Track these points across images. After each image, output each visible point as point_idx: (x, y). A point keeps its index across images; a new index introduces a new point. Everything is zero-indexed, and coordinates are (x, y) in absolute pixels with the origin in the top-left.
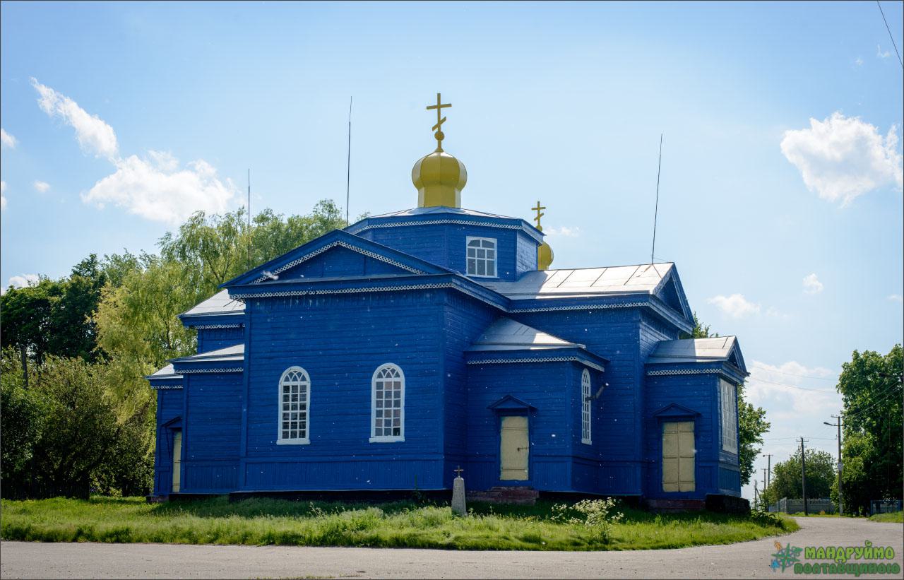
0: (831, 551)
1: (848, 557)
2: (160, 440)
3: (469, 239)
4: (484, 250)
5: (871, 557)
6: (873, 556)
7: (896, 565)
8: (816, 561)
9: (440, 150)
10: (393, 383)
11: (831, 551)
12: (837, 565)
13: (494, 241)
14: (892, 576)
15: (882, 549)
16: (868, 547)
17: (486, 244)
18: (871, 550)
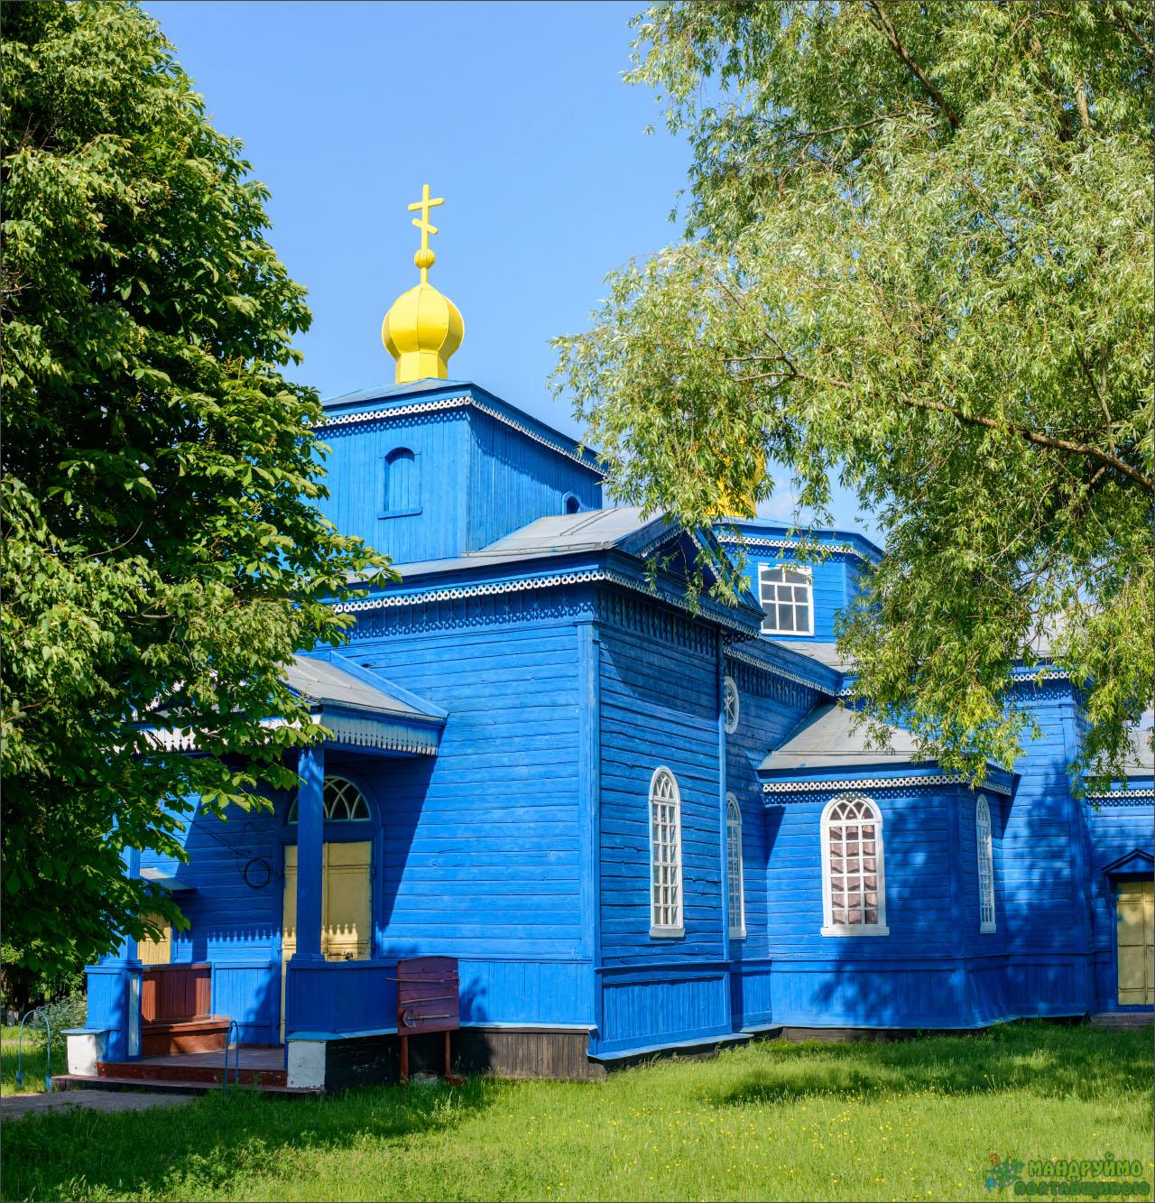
16: (1109, 1162)
18: (1112, 1164)
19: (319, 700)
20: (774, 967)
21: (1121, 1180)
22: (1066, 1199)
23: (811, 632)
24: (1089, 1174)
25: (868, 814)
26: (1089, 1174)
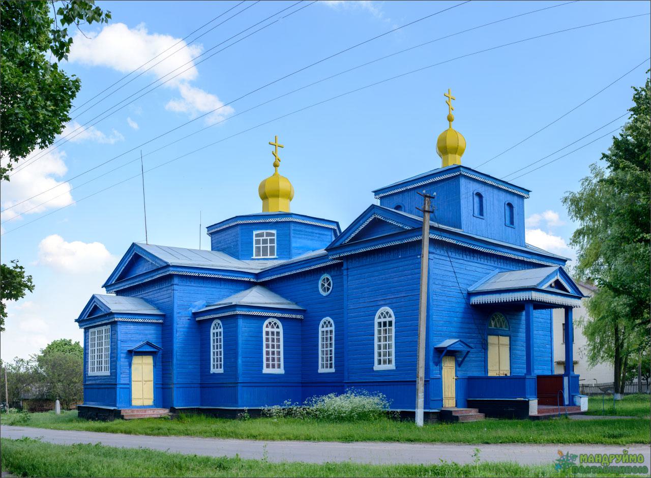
0: (598, 457)
1: (610, 461)
3: (255, 233)
11: (598, 457)
12: (602, 467)
13: (274, 232)
16: (625, 455)
17: (268, 234)
18: (627, 456)
20: (199, 386)
21: (632, 465)
22: (600, 476)
23: (275, 256)
24: (614, 461)
25: (278, 327)
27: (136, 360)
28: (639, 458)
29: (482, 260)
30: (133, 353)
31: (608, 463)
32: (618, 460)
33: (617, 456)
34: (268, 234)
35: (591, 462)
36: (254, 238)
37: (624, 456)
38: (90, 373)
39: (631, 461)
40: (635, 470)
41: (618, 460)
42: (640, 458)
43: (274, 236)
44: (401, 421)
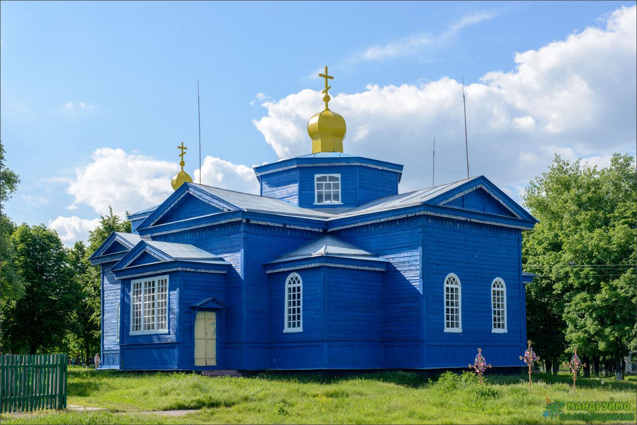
0: (585, 404)
1: (597, 409)
2: (123, 320)
3: (317, 176)
4: (329, 181)
5: (614, 409)
6: (615, 408)
7: (631, 414)
8: (575, 412)
9: (327, 109)
10: (450, 289)
11: (585, 404)
12: (589, 414)
13: (339, 176)
14: (628, 422)
15: (621, 403)
16: (612, 402)
17: (331, 179)
18: (613, 404)
19: (174, 258)
26: (601, 408)
27: (200, 316)
28: (625, 406)
29: (261, 231)
30: (197, 309)
31: (595, 410)
32: (604, 407)
33: (604, 404)
34: (331, 179)
35: (578, 409)
36: (316, 182)
37: (610, 403)
38: (132, 333)
39: (617, 408)
40: (623, 417)
41: (604, 407)
42: (626, 405)
43: (338, 181)
44: (612, 391)
